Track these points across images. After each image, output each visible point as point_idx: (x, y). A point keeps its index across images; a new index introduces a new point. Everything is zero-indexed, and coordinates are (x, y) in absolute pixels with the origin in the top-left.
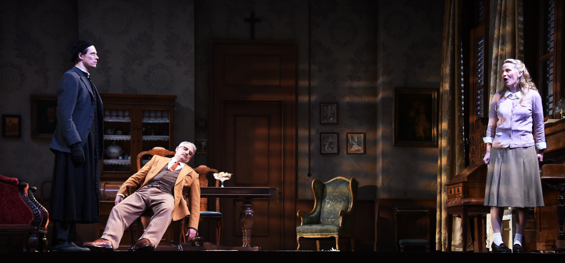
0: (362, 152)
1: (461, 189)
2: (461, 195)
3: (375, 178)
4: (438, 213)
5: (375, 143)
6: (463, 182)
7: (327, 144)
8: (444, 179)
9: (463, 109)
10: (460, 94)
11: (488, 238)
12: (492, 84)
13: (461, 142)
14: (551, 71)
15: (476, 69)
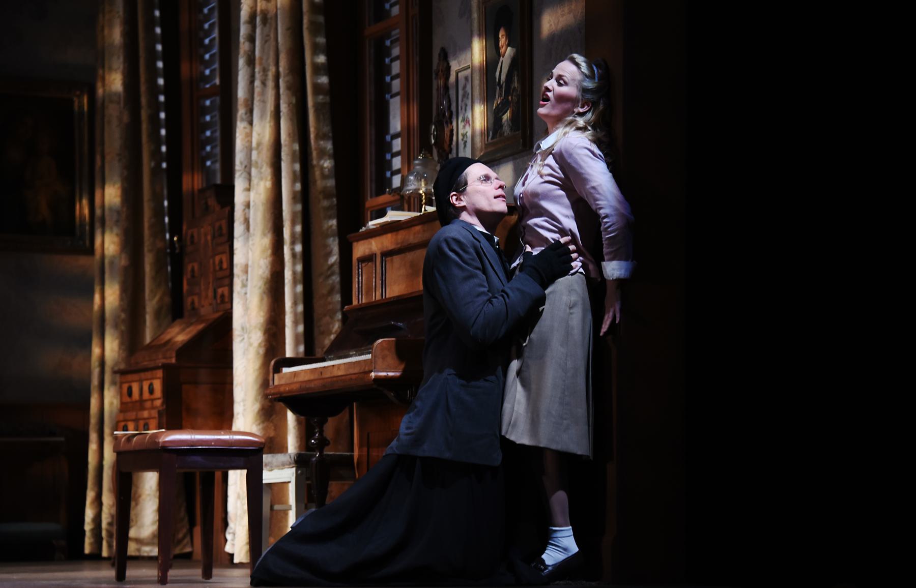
1: (157, 385)
2: (158, 403)
4: (93, 447)
6: (166, 368)
8: (111, 347)
9: (164, 149)
10: (155, 107)
11: (231, 525)
12: (241, 93)
13: (160, 244)
14: (396, 68)
15: (197, 47)
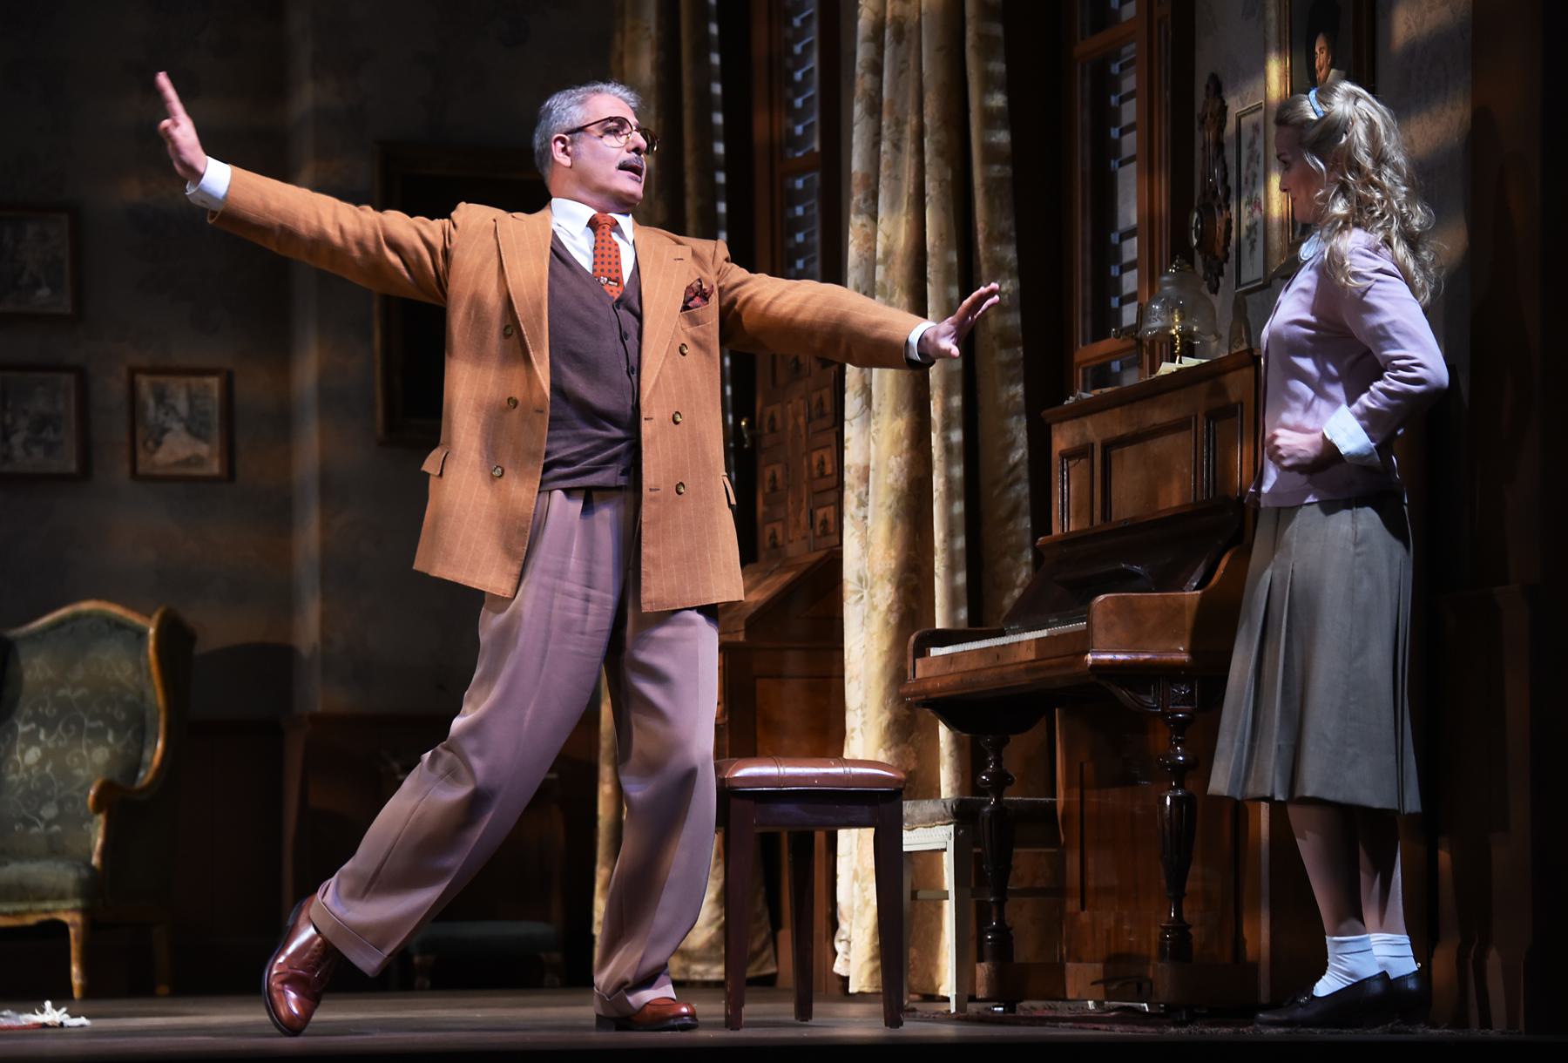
0: (215, 468)
3: (286, 604)
5: (283, 421)
7: (23, 423)
11: (844, 925)
12: (857, 163)
14: (1130, 112)
